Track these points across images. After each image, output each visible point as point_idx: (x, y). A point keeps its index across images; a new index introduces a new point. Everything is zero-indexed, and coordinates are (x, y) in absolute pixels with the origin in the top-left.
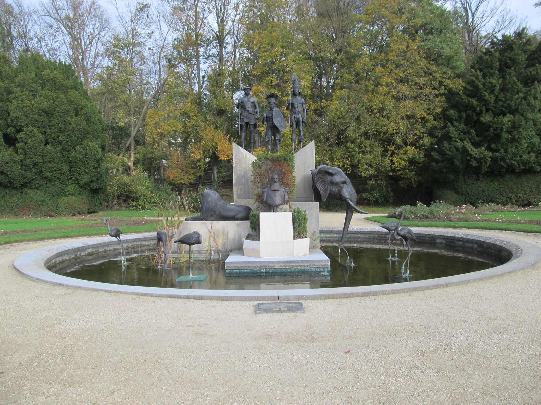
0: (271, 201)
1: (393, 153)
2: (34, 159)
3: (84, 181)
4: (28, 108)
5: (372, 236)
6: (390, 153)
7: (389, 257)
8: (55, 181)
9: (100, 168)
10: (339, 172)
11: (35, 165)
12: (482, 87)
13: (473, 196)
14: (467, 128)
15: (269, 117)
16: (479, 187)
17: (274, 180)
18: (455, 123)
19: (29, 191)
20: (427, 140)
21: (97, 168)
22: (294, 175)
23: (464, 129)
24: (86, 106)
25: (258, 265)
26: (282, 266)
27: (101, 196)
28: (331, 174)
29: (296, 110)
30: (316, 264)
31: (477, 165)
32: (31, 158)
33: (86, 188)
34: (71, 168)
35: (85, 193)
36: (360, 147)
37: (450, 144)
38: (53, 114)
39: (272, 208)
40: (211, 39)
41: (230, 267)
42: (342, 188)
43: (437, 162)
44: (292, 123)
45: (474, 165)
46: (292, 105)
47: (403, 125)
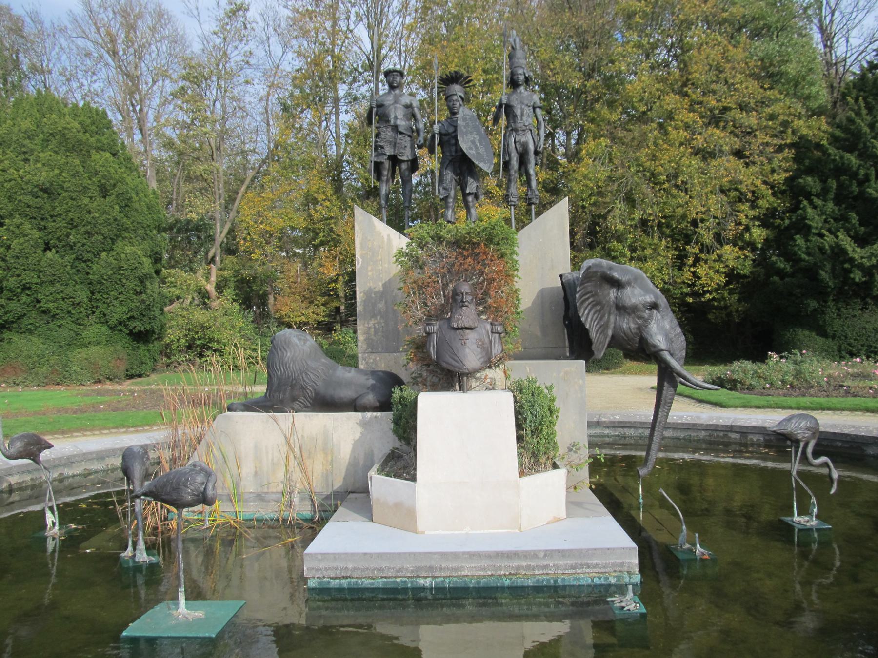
0: (451, 361)
1: (697, 260)
2: (23, 276)
3: (116, 317)
4: (13, 182)
5: (693, 434)
6: (691, 260)
7: (792, 515)
8: (63, 318)
9: (145, 293)
10: (636, 278)
11: (26, 288)
12: (868, 131)
13: (855, 340)
14: (839, 210)
15: (446, 135)
16: (868, 322)
17: (459, 298)
18: (815, 200)
19: (15, 338)
20: (758, 234)
21: (141, 293)
22: (517, 286)
23: (833, 211)
24: (122, 181)
25: (409, 566)
26: (484, 569)
27: (155, 346)
28: (618, 284)
29: (519, 125)
30: (595, 562)
31: (864, 279)
32: (18, 276)
33: (121, 331)
34: (92, 293)
35: (121, 340)
36: (633, 250)
37: (807, 240)
38: (59, 195)
39: (456, 379)
40: (360, 70)
41: (318, 570)
42: (646, 321)
43: (781, 273)
44: (509, 155)
45: (857, 280)
46: (509, 109)
47: (716, 204)
